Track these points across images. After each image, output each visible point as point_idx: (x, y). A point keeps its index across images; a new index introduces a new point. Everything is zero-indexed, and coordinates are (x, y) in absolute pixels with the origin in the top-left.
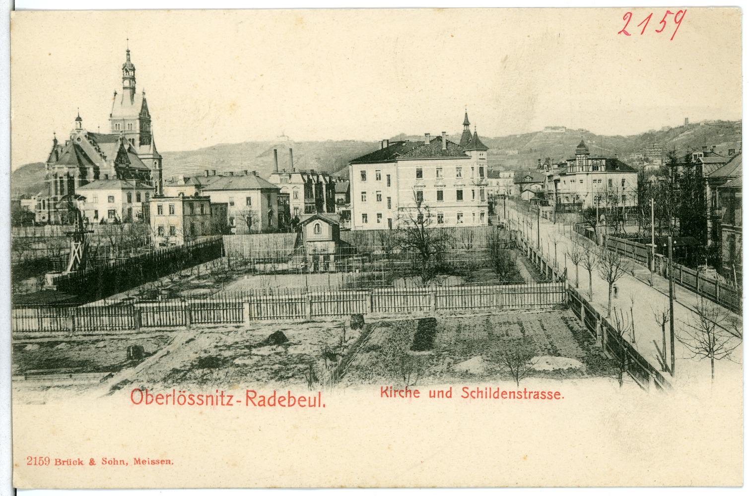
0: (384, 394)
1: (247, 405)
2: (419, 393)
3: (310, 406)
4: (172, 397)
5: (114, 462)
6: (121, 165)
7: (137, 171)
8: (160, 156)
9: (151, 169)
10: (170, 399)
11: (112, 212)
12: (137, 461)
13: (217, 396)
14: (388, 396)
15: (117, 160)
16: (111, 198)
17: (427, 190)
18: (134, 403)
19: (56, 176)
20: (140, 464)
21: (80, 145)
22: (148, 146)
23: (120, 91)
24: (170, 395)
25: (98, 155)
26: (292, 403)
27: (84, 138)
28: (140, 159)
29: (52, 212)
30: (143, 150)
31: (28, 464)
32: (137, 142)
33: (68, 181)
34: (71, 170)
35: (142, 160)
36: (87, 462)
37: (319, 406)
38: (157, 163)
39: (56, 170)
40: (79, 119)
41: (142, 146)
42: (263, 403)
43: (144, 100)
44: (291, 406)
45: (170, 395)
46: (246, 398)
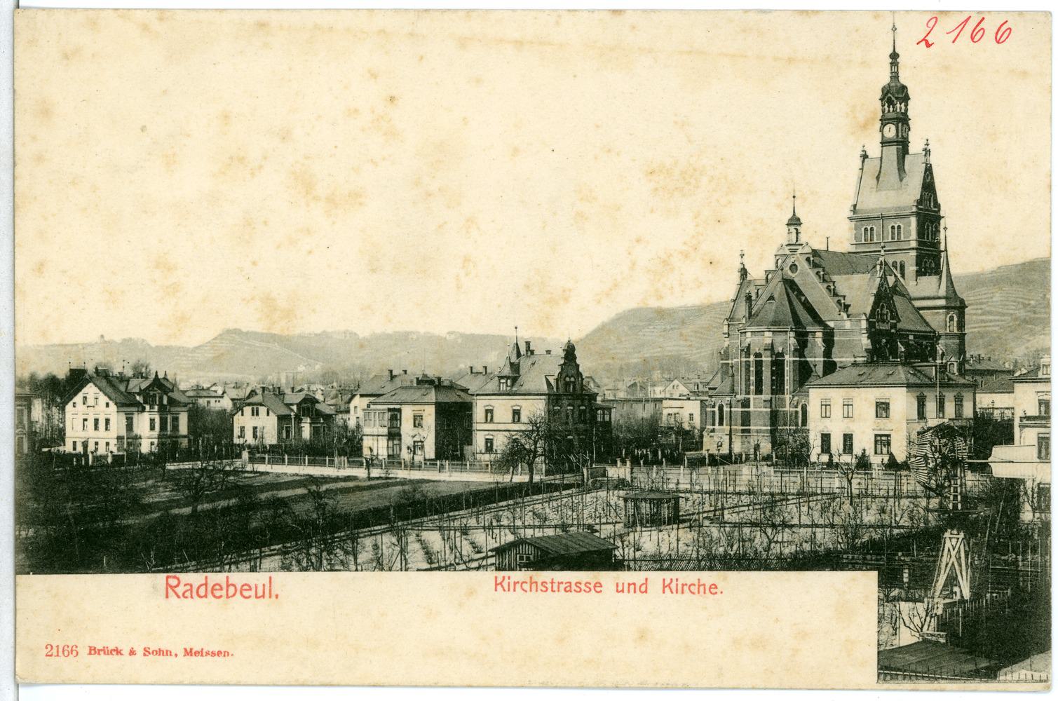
0: (499, 587)
2: (601, 586)
3: (257, 597)
7: (911, 337)
8: (962, 301)
9: (942, 332)
11: (883, 441)
12: (189, 652)
14: (504, 590)
16: (883, 408)
19: (747, 351)
21: (796, 280)
22: (934, 278)
23: (874, 150)
25: (832, 302)
27: (806, 265)
29: (736, 431)
30: (928, 287)
31: (47, 655)
32: (911, 269)
33: (772, 361)
34: (779, 339)
35: (921, 312)
36: (126, 651)
37: (270, 597)
38: (956, 319)
39: (749, 338)
40: (795, 222)
43: (929, 170)
46: (165, 586)
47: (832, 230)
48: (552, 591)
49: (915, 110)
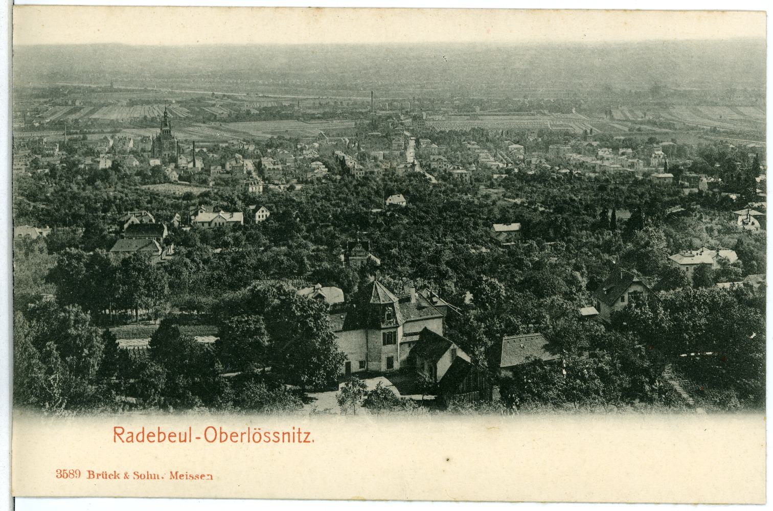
1: (115, 441)
3: (159, 441)
4: (247, 435)
5: (149, 476)
10: (245, 437)
12: (175, 476)
13: (294, 433)
18: (207, 440)
20: (177, 478)
24: (245, 433)
36: (122, 476)
42: (130, 439)
48: (180, 441)
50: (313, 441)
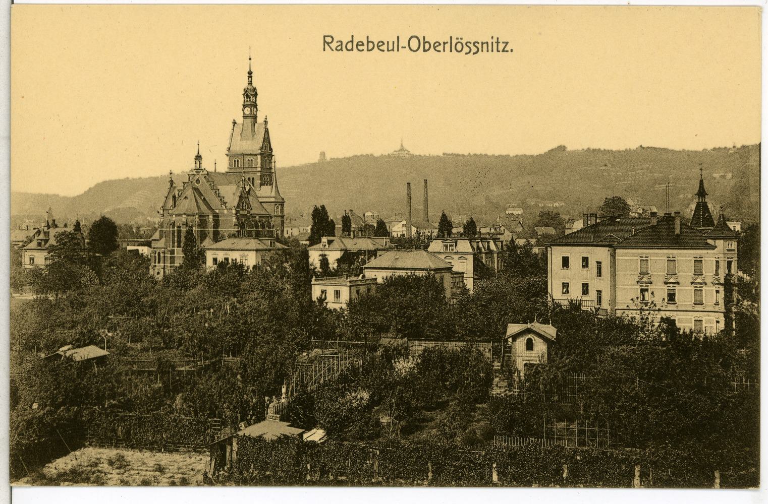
6: (242, 212)
8: (283, 199)
10: (448, 46)
15: (238, 207)
17: (680, 288)
22: (269, 187)
23: (240, 120)
26: (370, 47)
28: (261, 203)
30: (265, 192)
32: (257, 182)
41: (262, 187)
43: (267, 131)
44: (371, 50)
45: (447, 43)
47: (217, 161)
49: (260, 101)
50: (512, 51)
